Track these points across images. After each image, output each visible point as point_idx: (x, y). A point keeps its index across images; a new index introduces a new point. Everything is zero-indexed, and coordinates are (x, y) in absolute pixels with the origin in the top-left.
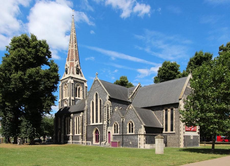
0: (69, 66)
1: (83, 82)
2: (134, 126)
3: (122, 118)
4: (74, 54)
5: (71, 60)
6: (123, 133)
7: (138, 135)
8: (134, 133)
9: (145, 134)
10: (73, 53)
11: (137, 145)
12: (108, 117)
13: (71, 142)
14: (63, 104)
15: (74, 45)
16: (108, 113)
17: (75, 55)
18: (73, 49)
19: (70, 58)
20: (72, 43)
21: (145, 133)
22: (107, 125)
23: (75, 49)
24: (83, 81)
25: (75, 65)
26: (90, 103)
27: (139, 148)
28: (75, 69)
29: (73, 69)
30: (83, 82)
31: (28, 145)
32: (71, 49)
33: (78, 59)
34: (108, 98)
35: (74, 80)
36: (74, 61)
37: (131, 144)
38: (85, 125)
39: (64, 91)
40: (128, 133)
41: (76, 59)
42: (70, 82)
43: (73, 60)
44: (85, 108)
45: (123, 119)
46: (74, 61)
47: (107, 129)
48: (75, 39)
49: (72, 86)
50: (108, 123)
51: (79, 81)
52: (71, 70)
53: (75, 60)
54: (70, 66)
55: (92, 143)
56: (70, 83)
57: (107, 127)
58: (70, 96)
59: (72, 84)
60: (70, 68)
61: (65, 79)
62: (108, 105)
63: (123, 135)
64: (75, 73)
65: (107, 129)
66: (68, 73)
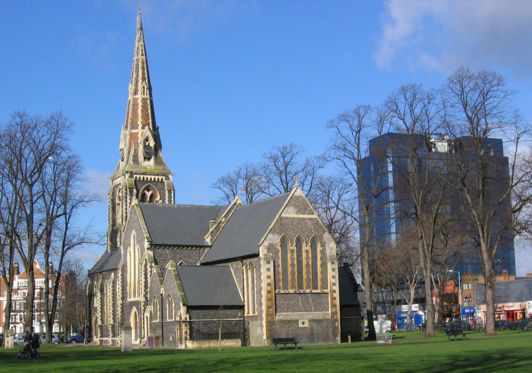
1: (162, 179)
7: (162, 323)
17: (143, 111)
23: (143, 97)
24: (160, 178)
25: (141, 139)
28: (141, 148)
30: (162, 179)
33: (150, 121)
35: (136, 178)
36: (139, 130)
38: (119, 302)
39: (117, 207)
40: (168, 320)
43: (137, 128)
44: (120, 266)
51: (149, 180)
53: (140, 126)
62: (146, 260)
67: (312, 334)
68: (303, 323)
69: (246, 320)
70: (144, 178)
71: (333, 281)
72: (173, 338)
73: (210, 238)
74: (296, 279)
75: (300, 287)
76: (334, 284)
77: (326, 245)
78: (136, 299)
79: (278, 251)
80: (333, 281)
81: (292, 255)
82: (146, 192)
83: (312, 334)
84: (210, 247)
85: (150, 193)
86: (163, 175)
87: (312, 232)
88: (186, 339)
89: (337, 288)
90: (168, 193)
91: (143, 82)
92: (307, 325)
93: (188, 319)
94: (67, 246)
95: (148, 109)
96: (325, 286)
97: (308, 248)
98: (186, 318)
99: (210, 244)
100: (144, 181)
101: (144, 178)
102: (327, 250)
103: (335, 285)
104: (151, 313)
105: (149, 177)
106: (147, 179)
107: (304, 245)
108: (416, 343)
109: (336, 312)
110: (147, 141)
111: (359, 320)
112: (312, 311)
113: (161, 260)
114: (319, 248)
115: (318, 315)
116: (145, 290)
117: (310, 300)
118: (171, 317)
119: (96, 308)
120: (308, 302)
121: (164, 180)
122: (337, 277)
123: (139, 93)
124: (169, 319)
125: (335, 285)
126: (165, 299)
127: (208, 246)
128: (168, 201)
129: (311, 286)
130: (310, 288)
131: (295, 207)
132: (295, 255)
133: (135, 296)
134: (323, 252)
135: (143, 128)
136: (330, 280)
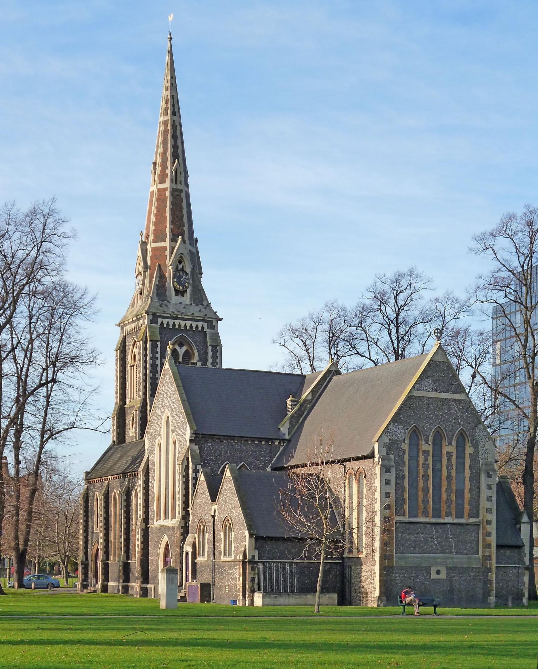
1: (203, 328)
18: (166, 189)
23: (174, 186)
24: (200, 324)
30: (203, 328)
33: (186, 228)
35: (162, 324)
67: (451, 591)
68: (438, 572)
69: (347, 563)
70: (174, 325)
71: (488, 505)
72: (230, 587)
73: (287, 425)
74: (430, 500)
75: (460, 515)
76: (489, 511)
77: (481, 444)
79: (404, 452)
80: (488, 505)
81: (426, 460)
82: (177, 348)
83: (451, 591)
84: (289, 441)
85: (184, 348)
86: (204, 321)
87: (459, 424)
88: (253, 591)
89: (492, 517)
90: (212, 350)
91: (174, 162)
92: (443, 576)
93: (257, 559)
94: (48, 433)
96: (475, 512)
97: (452, 449)
98: (253, 557)
99: (287, 437)
100: (175, 330)
101: (174, 325)
102: (480, 454)
103: (490, 512)
104: (194, 546)
105: (183, 323)
106: (180, 325)
107: (445, 443)
108: (28, 629)
109: (490, 556)
110: (180, 262)
111: (520, 571)
112: (451, 553)
113: (212, 460)
114: (469, 450)
115: (460, 559)
117: (450, 535)
118: (227, 553)
120: (447, 538)
121: (206, 329)
122: (494, 499)
125: (490, 512)
127: (284, 440)
128: (212, 363)
129: (454, 513)
130: (451, 515)
131: (434, 381)
132: (430, 459)
133: (166, 517)
134: (474, 457)
135: (174, 240)
136: (484, 504)
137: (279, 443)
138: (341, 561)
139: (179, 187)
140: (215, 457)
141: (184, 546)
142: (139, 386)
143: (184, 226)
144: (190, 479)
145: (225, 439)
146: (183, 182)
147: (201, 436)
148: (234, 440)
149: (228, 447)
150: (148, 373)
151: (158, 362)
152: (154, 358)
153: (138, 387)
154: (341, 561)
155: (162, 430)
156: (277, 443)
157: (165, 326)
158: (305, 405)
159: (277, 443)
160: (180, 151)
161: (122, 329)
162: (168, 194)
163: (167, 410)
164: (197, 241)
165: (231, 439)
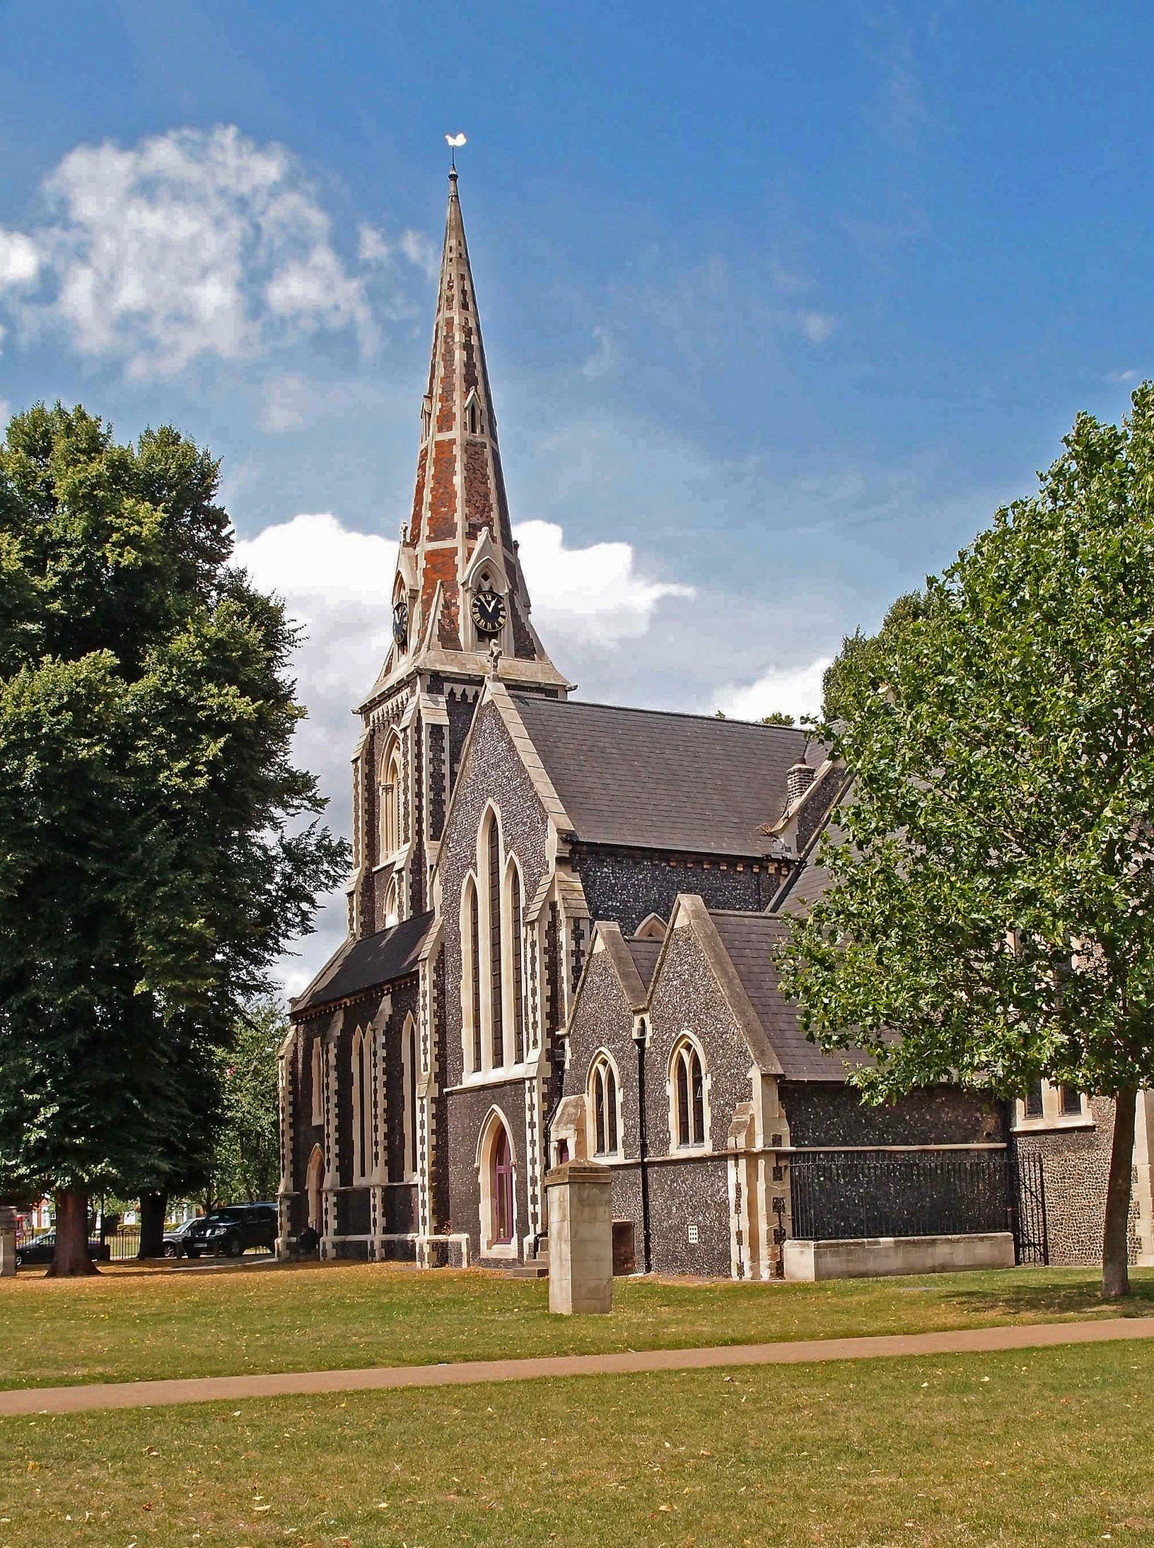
0: (421, 581)
2: (707, 1084)
3: (636, 1012)
4: (458, 480)
5: (432, 530)
6: (644, 1148)
8: (707, 1149)
9: (787, 1147)
10: (454, 473)
11: (726, 1256)
12: (554, 1017)
13: (377, 1245)
14: (382, 908)
15: (459, 405)
16: (554, 981)
17: (469, 482)
18: (452, 442)
19: (426, 514)
20: (447, 397)
21: (786, 1140)
22: (545, 1081)
25: (464, 572)
26: (456, 897)
27: (735, 1277)
28: (464, 603)
29: (447, 606)
31: (46, 1281)
32: (439, 444)
33: (495, 514)
34: (552, 846)
35: (452, 694)
37: (692, 1249)
40: (677, 1151)
41: (474, 520)
42: (419, 719)
43: (451, 533)
45: (643, 1022)
46: (458, 542)
47: (548, 1114)
48: (470, 357)
49: (436, 748)
50: (558, 1066)
52: (435, 613)
54: (430, 584)
55: (474, 1246)
56: (418, 730)
57: (545, 1097)
58: (419, 833)
59: (436, 730)
60: (427, 604)
61: (389, 696)
62: (553, 906)
63: (644, 1166)
64: (465, 634)
65: (548, 1114)
66: (413, 642)
78: (510, 1071)
91: (468, 391)
95: (485, 476)
116: (550, 1033)
119: (321, 1127)
123: (457, 424)
124: (684, 1139)
126: (653, 1056)
135: (471, 534)
137: (778, 870)
138: (1004, 1145)
139: (479, 437)
140: (624, 902)
141: (552, 1128)
142: (406, 819)
143: (491, 510)
144: (563, 955)
145: (647, 858)
146: (486, 429)
147: (585, 848)
148: (668, 861)
149: (654, 879)
150: (424, 791)
151: (446, 769)
152: (436, 761)
153: (402, 822)
154: (1004, 1145)
155: (478, 852)
156: (772, 870)
157: (458, 697)
158: (833, 781)
159: (772, 870)
160: (478, 373)
161: (367, 719)
162: (457, 450)
163: (490, 801)
164: (516, 546)
165: (661, 860)
